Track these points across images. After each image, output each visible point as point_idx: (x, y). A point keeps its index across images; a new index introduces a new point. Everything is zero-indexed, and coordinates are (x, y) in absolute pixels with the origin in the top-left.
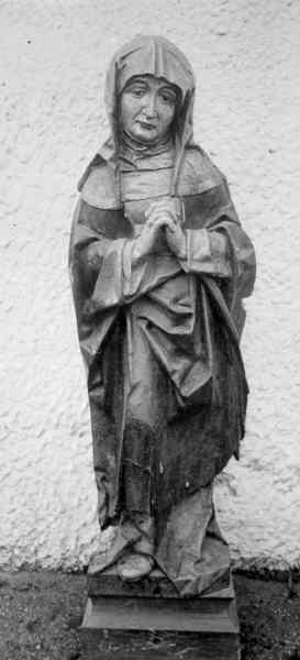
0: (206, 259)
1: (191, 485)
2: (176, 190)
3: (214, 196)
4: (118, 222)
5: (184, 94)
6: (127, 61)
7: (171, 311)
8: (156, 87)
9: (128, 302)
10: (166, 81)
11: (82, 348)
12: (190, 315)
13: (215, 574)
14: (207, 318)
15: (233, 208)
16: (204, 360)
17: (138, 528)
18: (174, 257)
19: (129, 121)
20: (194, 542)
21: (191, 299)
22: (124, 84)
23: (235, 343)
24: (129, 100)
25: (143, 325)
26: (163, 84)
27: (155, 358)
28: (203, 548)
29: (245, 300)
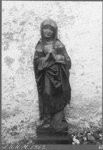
0: (60, 60)
1: (59, 109)
2: (54, 47)
3: (62, 49)
4: (43, 54)
5: (55, 28)
6: (44, 23)
7: (53, 71)
8: (49, 27)
9: (45, 69)
10: (51, 26)
11: (36, 80)
12: (57, 71)
13: (64, 128)
14: (61, 76)
15: (66, 51)
16: (60, 81)
17: (47, 117)
18: (54, 60)
19: (45, 34)
20: (60, 121)
21: (57, 68)
22: (43, 27)
23: (68, 80)
24: (45, 30)
25: (48, 74)
26: (51, 27)
27: (50, 81)
28: (62, 122)
29: (69, 70)
